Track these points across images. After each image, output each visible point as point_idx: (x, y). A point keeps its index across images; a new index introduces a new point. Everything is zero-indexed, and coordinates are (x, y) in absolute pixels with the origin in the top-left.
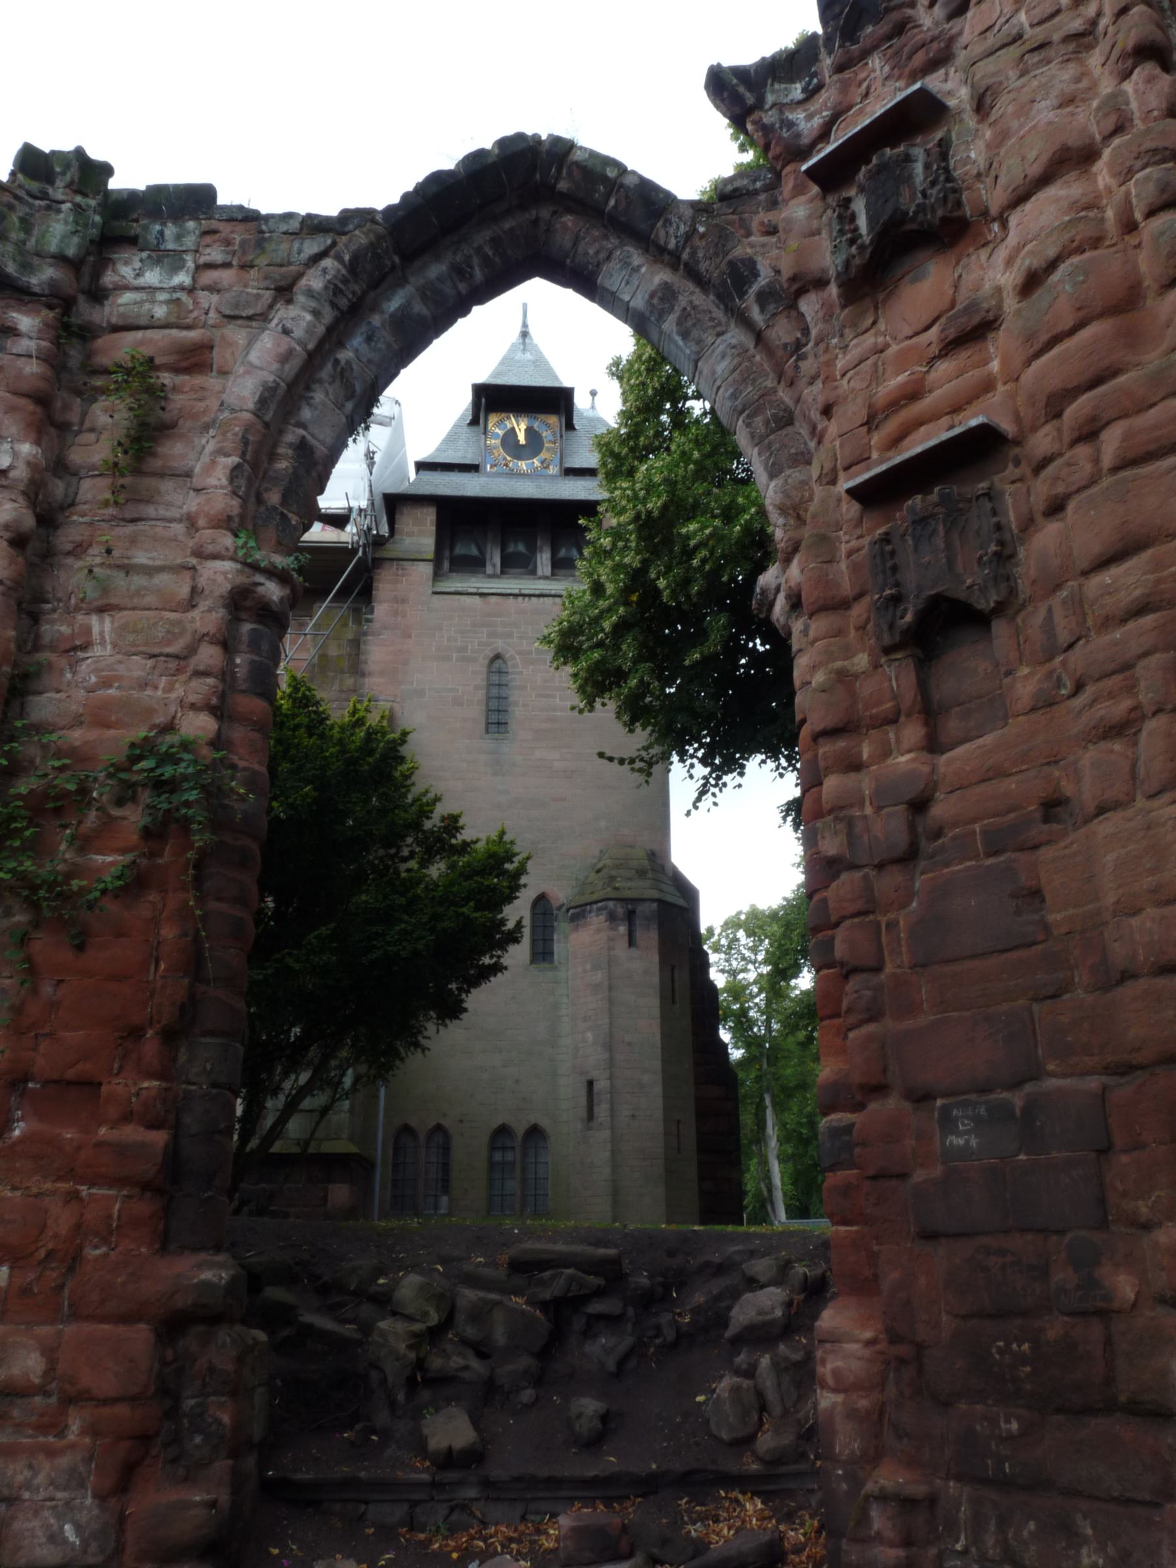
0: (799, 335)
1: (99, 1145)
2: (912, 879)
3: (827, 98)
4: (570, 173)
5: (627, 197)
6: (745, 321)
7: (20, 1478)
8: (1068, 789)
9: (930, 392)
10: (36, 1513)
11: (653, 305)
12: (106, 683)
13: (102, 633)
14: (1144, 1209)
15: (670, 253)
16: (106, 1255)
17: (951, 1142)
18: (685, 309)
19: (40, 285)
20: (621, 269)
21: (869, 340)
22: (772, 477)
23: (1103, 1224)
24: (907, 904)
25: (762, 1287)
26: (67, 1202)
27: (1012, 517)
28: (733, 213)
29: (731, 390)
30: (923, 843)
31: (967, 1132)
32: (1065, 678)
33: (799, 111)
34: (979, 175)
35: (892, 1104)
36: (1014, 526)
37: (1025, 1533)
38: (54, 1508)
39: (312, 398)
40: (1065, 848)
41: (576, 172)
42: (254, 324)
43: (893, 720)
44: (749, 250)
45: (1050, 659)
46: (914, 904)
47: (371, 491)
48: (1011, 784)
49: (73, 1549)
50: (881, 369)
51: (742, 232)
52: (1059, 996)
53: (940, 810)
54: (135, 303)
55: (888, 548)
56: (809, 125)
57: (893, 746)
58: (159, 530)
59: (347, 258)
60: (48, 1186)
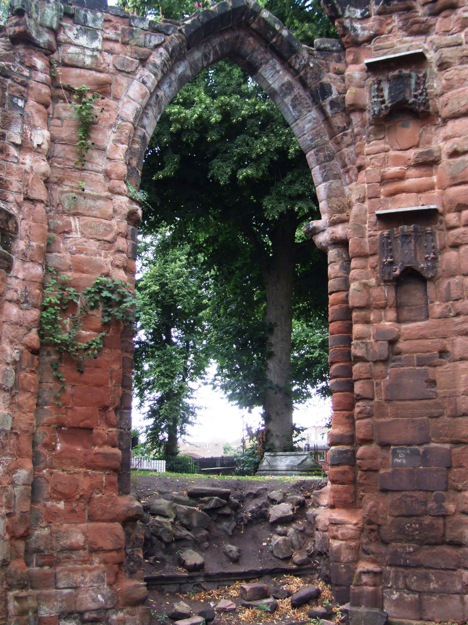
0: (345, 125)
1: (96, 454)
2: (387, 369)
3: (372, 23)
4: (259, 22)
5: (282, 40)
6: (322, 110)
7: (79, 580)
8: (449, 348)
9: (407, 178)
10: (87, 591)
11: (282, 90)
12: (80, 251)
13: (76, 226)
14: (460, 486)
15: (295, 70)
16: (101, 497)
18: (296, 96)
19: (44, 43)
20: (271, 69)
21: (381, 145)
22: (324, 180)
23: (446, 490)
24: (384, 378)
25: (279, 503)
26: (85, 476)
28: (323, 59)
29: (310, 137)
30: (391, 355)
31: (402, 458)
32: (452, 309)
33: (358, 23)
34: (436, 95)
36: (438, 247)
37: (412, 580)
38: (93, 589)
39: (148, 113)
41: (262, 22)
42: (130, 76)
43: (383, 308)
44: (329, 80)
45: (448, 301)
46: (388, 378)
48: (428, 342)
49: (102, 603)
51: (326, 70)
53: (401, 345)
54: (76, 54)
55: (389, 241)
56: (362, 33)
57: (383, 317)
58: (93, 176)
59: (170, 49)
60: (77, 470)
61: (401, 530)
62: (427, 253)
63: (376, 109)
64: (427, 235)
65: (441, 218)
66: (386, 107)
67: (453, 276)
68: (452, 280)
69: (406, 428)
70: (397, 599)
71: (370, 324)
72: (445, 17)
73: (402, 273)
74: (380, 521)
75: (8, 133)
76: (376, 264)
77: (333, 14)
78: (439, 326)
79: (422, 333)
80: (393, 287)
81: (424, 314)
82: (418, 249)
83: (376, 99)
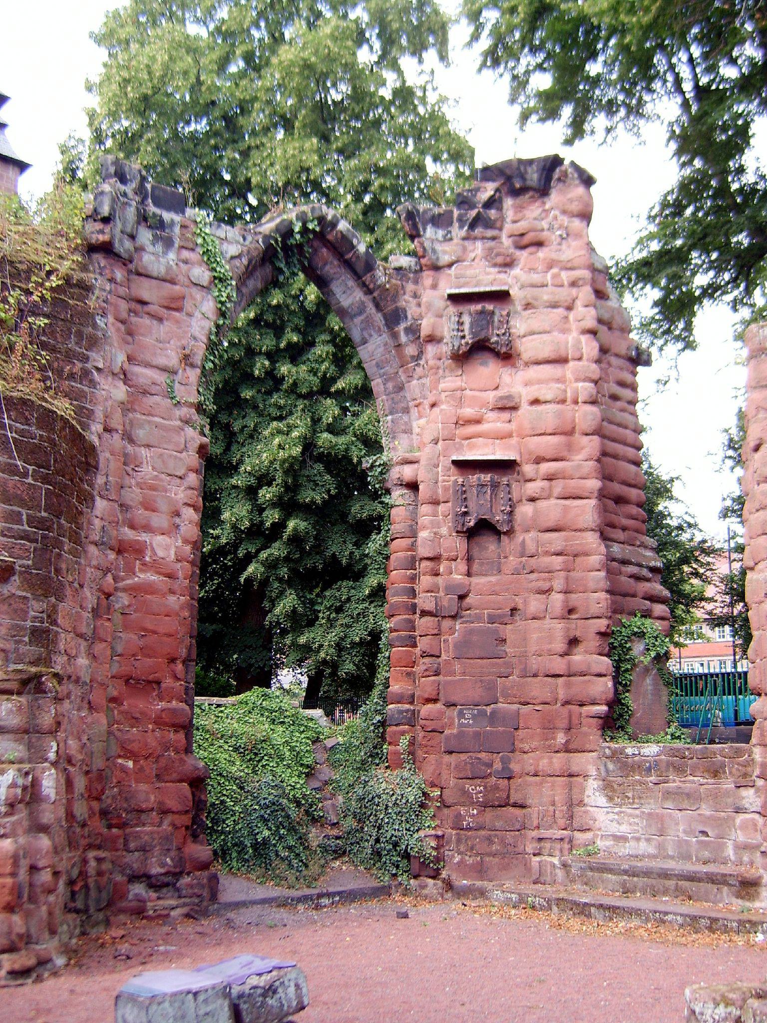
8: (520, 606)
15: (368, 289)
35: (439, 706)
40: (47, 401)
53: (468, 600)
61: (465, 793)
63: (456, 344)
66: (467, 343)
67: (528, 531)
72: (531, 254)
73: (476, 524)
74: (443, 784)
75: (92, 355)
77: (414, 233)
78: (511, 583)
83: (455, 333)
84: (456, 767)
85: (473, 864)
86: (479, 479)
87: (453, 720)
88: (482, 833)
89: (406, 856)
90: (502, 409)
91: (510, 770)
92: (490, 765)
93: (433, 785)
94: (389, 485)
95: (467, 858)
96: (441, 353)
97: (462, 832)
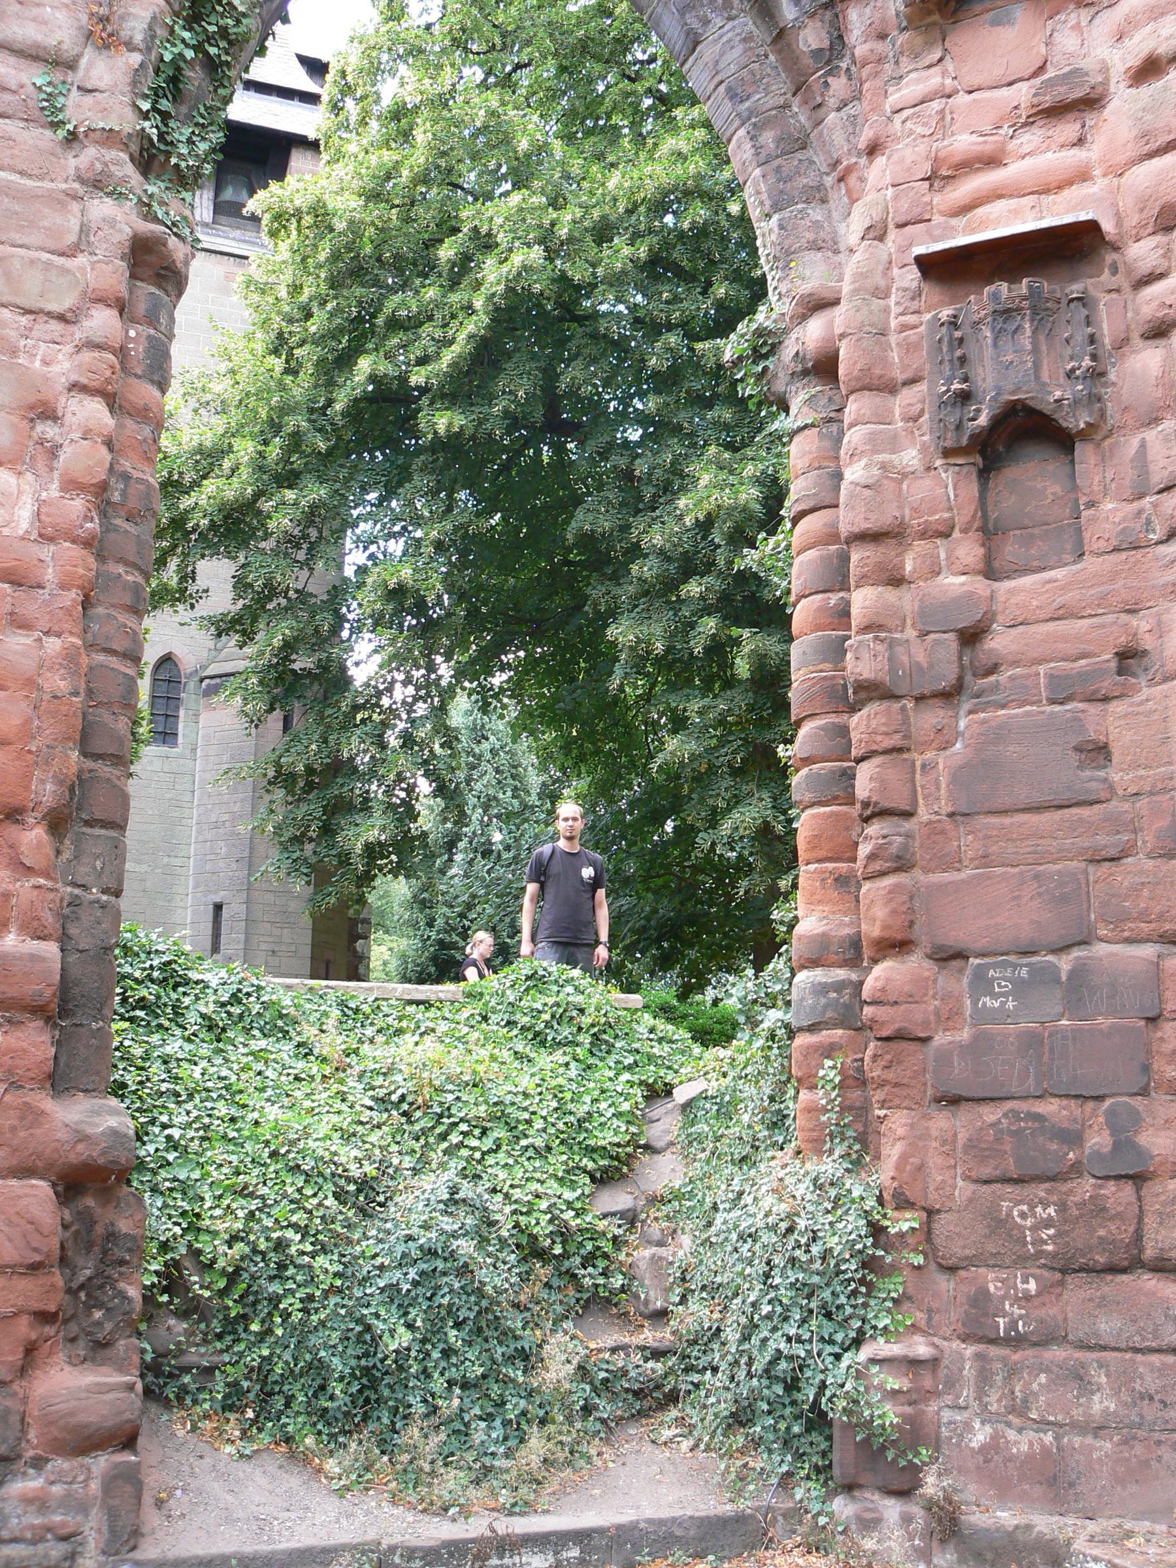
2: (956, 717)
8: (1148, 642)
17: (984, 1004)
23: (1144, 1092)
27: (1107, 331)
30: (969, 678)
31: (1001, 995)
36: (1107, 341)
45: (1141, 496)
46: (958, 745)
47: (1093, 18)
50: (948, 118)
52: (1119, 859)
53: (999, 642)
55: (958, 334)
61: (1000, 1225)
62: (1072, 359)
64: (1072, 305)
65: (1110, 257)
68: (1151, 435)
69: (1018, 897)
70: (983, 1449)
71: (905, 587)
76: (919, 406)
78: (1113, 576)
79: (1060, 600)
80: (974, 469)
81: (1069, 546)
82: (1044, 348)
84: (970, 1146)
85: (1030, 1457)
86: (995, 297)
87: (959, 1000)
88: (1057, 1353)
89: (818, 1420)
90: (1055, 112)
91: (1141, 1154)
92: (1073, 1138)
93: (903, 1203)
94: (779, 386)
95: (1012, 1435)
96: (883, 20)
97: (994, 1351)
